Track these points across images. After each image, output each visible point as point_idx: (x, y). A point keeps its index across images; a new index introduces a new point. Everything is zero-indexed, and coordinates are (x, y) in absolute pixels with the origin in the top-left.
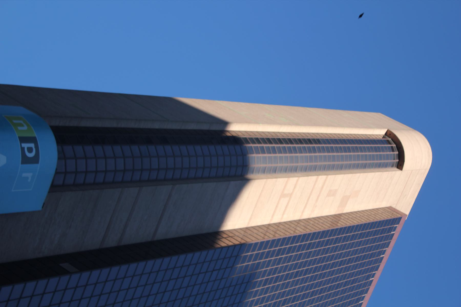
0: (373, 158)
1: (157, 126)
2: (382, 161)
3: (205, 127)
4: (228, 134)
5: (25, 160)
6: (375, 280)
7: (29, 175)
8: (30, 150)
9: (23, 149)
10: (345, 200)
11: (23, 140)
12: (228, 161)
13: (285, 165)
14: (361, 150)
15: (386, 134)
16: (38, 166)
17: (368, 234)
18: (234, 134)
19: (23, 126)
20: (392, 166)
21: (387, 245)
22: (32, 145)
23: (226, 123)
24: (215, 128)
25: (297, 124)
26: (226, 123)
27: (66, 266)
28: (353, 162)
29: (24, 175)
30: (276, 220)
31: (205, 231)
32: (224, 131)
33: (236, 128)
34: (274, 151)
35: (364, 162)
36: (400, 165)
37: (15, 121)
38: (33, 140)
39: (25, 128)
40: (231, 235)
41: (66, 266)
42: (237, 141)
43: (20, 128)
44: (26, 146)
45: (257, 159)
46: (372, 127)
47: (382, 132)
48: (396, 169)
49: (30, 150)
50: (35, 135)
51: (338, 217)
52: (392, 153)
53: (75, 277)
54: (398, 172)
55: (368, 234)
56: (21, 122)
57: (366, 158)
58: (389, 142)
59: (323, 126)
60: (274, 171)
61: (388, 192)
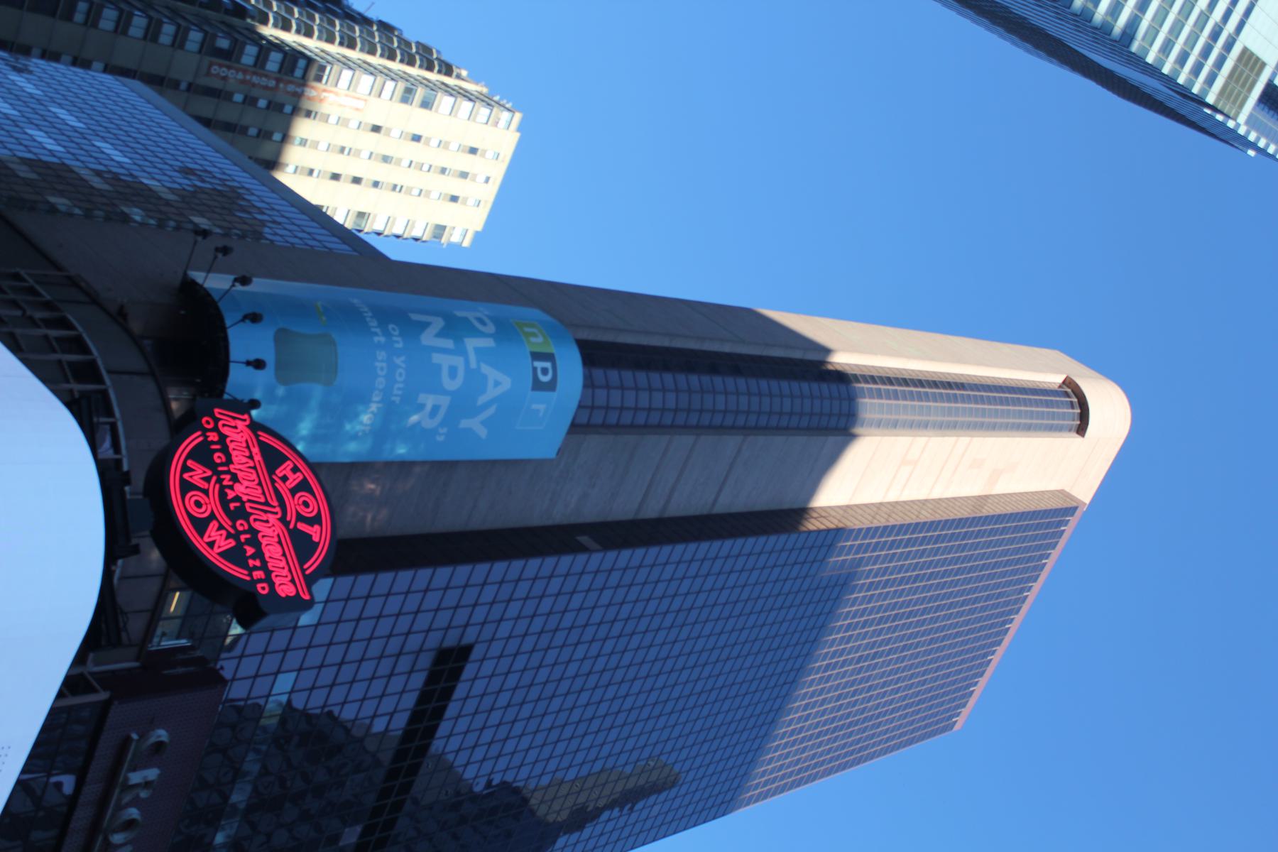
0: (1041, 415)
3: (797, 355)
4: (830, 367)
5: (538, 386)
7: (542, 407)
8: (545, 371)
9: (535, 369)
11: (536, 356)
15: (1064, 382)
18: (839, 368)
22: (548, 365)
23: (827, 351)
26: (827, 351)
29: (534, 406)
31: (786, 506)
32: (823, 363)
33: (841, 359)
36: (1082, 429)
37: (527, 329)
38: (549, 357)
39: (540, 339)
41: (584, 539)
42: (842, 378)
43: (533, 339)
45: (869, 406)
46: (1044, 369)
47: (1059, 379)
49: (545, 371)
50: (551, 348)
53: (596, 557)
54: (1079, 439)
57: (1031, 415)
61: (1063, 468)
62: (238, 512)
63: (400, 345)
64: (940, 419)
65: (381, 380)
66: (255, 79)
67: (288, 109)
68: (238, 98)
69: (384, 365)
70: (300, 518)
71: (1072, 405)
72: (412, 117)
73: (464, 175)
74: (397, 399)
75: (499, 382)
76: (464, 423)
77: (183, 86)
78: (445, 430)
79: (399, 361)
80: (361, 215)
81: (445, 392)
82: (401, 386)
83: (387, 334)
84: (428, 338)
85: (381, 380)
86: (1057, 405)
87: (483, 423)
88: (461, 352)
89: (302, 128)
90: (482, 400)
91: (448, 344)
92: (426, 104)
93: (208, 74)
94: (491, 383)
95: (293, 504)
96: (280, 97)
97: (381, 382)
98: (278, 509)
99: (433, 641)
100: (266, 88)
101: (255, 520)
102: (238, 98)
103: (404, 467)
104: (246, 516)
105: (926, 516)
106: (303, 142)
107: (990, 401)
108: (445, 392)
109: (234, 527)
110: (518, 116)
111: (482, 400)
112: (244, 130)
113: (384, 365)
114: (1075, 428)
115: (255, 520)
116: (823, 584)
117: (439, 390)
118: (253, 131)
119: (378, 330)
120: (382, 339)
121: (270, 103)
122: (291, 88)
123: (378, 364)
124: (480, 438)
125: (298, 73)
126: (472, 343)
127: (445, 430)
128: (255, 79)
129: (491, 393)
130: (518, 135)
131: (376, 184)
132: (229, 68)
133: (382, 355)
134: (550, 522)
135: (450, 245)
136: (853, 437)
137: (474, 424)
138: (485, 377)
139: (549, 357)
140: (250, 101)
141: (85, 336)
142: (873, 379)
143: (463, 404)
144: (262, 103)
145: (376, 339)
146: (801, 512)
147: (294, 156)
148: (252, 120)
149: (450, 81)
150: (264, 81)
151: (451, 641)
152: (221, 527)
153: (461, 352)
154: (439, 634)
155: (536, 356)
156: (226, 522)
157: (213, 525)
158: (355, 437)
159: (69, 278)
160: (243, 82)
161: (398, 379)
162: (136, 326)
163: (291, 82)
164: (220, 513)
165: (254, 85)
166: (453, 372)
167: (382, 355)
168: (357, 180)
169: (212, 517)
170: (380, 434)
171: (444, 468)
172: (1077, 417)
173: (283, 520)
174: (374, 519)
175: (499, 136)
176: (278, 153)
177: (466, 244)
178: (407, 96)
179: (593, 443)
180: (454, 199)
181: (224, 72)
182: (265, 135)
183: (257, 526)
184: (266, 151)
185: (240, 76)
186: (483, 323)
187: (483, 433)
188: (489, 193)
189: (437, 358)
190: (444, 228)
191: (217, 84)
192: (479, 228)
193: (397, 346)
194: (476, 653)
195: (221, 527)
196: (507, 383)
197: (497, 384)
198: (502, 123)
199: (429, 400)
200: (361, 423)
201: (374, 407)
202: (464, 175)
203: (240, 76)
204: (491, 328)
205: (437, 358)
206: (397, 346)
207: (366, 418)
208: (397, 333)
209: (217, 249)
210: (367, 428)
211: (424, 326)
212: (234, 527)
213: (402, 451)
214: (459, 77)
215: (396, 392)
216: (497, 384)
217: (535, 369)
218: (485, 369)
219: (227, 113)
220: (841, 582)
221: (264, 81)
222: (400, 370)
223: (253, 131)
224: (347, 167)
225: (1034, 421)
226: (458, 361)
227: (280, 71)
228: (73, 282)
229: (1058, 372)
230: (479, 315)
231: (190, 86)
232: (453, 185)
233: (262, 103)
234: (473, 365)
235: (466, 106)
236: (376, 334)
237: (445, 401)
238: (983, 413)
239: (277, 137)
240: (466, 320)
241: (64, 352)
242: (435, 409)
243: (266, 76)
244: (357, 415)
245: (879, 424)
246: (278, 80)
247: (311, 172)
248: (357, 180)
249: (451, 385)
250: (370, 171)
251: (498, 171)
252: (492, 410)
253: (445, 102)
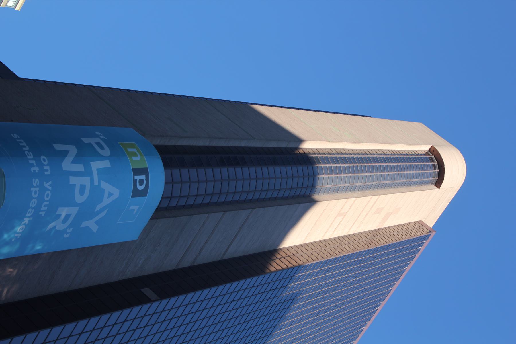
1: (243, 144)
2: (425, 179)
4: (301, 151)
5: (137, 193)
7: (136, 208)
9: (135, 181)
10: (387, 216)
11: (137, 171)
12: (291, 175)
13: (347, 185)
15: (429, 150)
16: (146, 198)
17: (401, 251)
18: (306, 152)
19: (136, 155)
20: (432, 184)
21: (412, 259)
22: (143, 177)
23: (300, 141)
25: (360, 141)
26: (300, 141)
27: (147, 292)
28: (402, 181)
29: (132, 208)
30: (327, 237)
31: (266, 250)
32: (297, 149)
33: (308, 146)
34: (339, 171)
35: (411, 180)
36: (438, 183)
37: (130, 150)
38: (143, 171)
39: (138, 158)
42: (307, 160)
43: (134, 158)
44: (138, 178)
45: (324, 180)
46: (411, 138)
47: (426, 148)
48: (434, 186)
50: (146, 165)
51: (375, 232)
52: (434, 171)
53: (155, 304)
54: (436, 190)
55: (401, 251)
56: (134, 150)
57: (412, 176)
58: (431, 160)
59: (380, 143)
60: (335, 191)
61: (420, 207)
63: (49, 173)
65: (35, 200)
71: (434, 167)
74: (43, 213)
75: (111, 192)
76: (85, 224)
79: (47, 185)
82: (47, 203)
83: (40, 165)
84: (67, 165)
85: (35, 200)
88: (88, 173)
90: (99, 207)
91: (80, 168)
94: (106, 194)
97: (34, 203)
103: (36, 257)
105: (347, 250)
111: (99, 207)
113: (37, 189)
114: (434, 182)
116: (283, 300)
119: (33, 162)
120: (36, 169)
123: (33, 189)
126: (97, 165)
129: (106, 201)
135: (7, 8)
136: (314, 202)
137: (91, 225)
138: (103, 191)
139: (143, 171)
143: (86, 211)
145: (32, 169)
146: (272, 253)
153: (88, 173)
155: (137, 171)
161: (46, 199)
166: (83, 188)
167: (36, 182)
170: (26, 239)
172: (436, 175)
174: (8, 291)
186: (102, 148)
187: (95, 228)
189: (73, 180)
193: (46, 173)
196: (116, 193)
197: (110, 194)
199: (64, 212)
201: (26, 220)
204: (107, 152)
205: (73, 180)
206: (46, 173)
207: (18, 229)
211: (64, 154)
213: (39, 247)
215: (43, 208)
216: (110, 194)
217: (135, 181)
218: (104, 185)
220: (293, 297)
222: (48, 192)
225: (414, 180)
226: (86, 181)
229: (426, 144)
234: (96, 183)
237: (74, 211)
238: (387, 177)
240: (90, 145)
242: (68, 216)
244: (13, 228)
245: (328, 191)
249: (79, 199)
252: (104, 214)
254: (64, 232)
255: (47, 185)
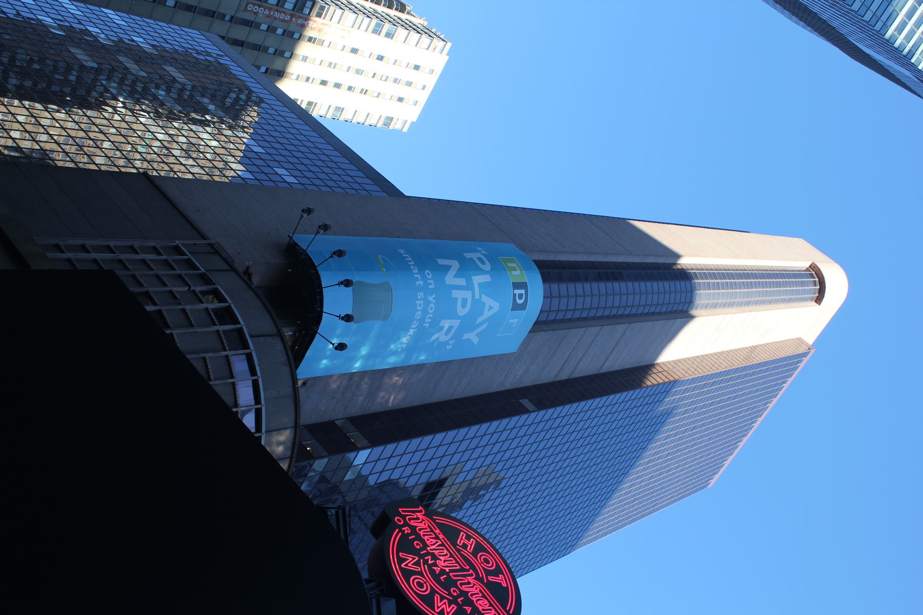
0: (798, 292)
3: (661, 260)
4: (679, 267)
5: (516, 307)
6: (771, 406)
8: (520, 296)
9: (515, 295)
11: (517, 286)
12: (668, 289)
14: (790, 284)
18: (684, 267)
22: (523, 291)
23: (678, 256)
24: (669, 261)
26: (678, 256)
27: (525, 402)
29: (511, 321)
32: (675, 264)
33: (686, 262)
36: (819, 300)
37: (510, 265)
38: (523, 286)
39: (518, 273)
40: (666, 369)
41: (525, 402)
42: (685, 276)
43: (514, 273)
44: (517, 292)
45: (702, 296)
46: (794, 254)
47: (807, 265)
49: (520, 298)
50: (525, 279)
53: (533, 415)
57: (792, 292)
58: (812, 276)
61: (798, 324)
62: (449, 584)
64: (741, 300)
66: (277, 15)
67: (296, 36)
68: (264, 27)
69: (422, 302)
70: (488, 573)
72: (380, 44)
73: (409, 84)
74: (427, 325)
75: (492, 306)
76: (466, 336)
77: (227, 18)
78: (453, 342)
79: (431, 298)
80: (338, 109)
81: (458, 317)
83: (425, 279)
84: (450, 279)
85: (419, 313)
86: (802, 284)
87: (477, 335)
88: (469, 287)
89: (303, 48)
90: (479, 320)
91: (462, 282)
92: (389, 35)
93: (245, 10)
94: (487, 308)
95: (478, 562)
96: (292, 28)
98: (471, 571)
99: (425, 478)
100: (283, 20)
101: (461, 584)
102: (264, 27)
103: (420, 367)
104: (454, 583)
105: (724, 366)
106: (305, 59)
107: (771, 285)
108: (458, 317)
109: (450, 594)
110: (449, 45)
111: (479, 320)
112: (266, 49)
113: (422, 302)
115: (461, 584)
117: (454, 316)
118: (271, 50)
119: (418, 276)
120: (421, 283)
121: (285, 31)
122: (300, 21)
123: (418, 302)
124: (476, 344)
125: (306, 11)
126: (478, 279)
127: (453, 342)
128: (277, 15)
129: (487, 314)
130: (447, 58)
131: (350, 88)
132: (260, 6)
133: (421, 295)
134: (503, 389)
135: (394, 131)
137: (472, 337)
139: (523, 286)
140: (271, 29)
141: (232, 306)
142: (705, 276)
143: (468, 324)
144: (280, 31)
145: (417, 283)
147: (295, 67)
148: (272, 43)
149: (404, 16)
150: (282, 16)
151: (435, 477)
152: (442, 598)
153: (469, 287)
154: (429, 474)
155: (517, 286)
156: (444, 592)
157: (437, 598)
158: (394, 353)
159: (211, 245)
160: (268, 16)
162: (256, 280)
163: (301, 17)
164: (437, 587)
165: (275, 19)
166: (464, 301)
167: (421, 295)
168: (337, 86)
169: (433, 592)
170: (411, 349)
171: (444, 366)
172: (817, 291)
173: (478, 578)
174: (394, 398)
175: (434, 58)
176: (285, 66)
177: (405, 130)
178: (377, 31)
179: (541, 336)
180: (400, 100)
181: (256, 9)
182: (279, 53)
183: (464, 588)
184: (277, 65)
185: (267, 12)
186: (484, 263)
188: (423, 97)
189: (455, 294)
190: (392, 119)
191: (251, 17)
192: (415, 120)
193: (430, 287)
194: (447, 483)
195: (442, 598)
196: (496, 306)
197: (491, 308)
198: (438, 50)
199: (446, 324)
200: (402, 343)
201: (411, 332)
202: (409, 84)
203: (267, 12)
206: (430, 287)
207: (404, 340)
208: (430, 277)
209: (303, 211)
210: (404, 346)
211: (447, 268)
212: (450, 594)
213: (422, 358)
214: (408, 13)
215: (427, 320)
216: (491, 308)
217: (515, 295)
218: (485, 298)
219: (255, 37)
221: (282, 16)
223: (271, 50)
224: (332, 76)
226: (468, 294)
227: (293, 9)
228: (215, 250)
230: (479, 255)
231: (232, 17)
232: (401, 90)
233: (280, 31)
234: (477, 297)
235: (414, 36)
236: (417, 279)
237: (456, 323)
239: (287, 54)
241: (222, 323)
242: (450, 328)
243: (284, 13)
244: (399, 339)
245: (706, 306)
246: (292, 16)
247: (308, 79)
248: (337, 86)
249: (461, 312)
250: (347, 79)
251: (431, 81)
252: (484, 326)
253: (401, 33)
254: (447, 343)
255: (431, 298)
